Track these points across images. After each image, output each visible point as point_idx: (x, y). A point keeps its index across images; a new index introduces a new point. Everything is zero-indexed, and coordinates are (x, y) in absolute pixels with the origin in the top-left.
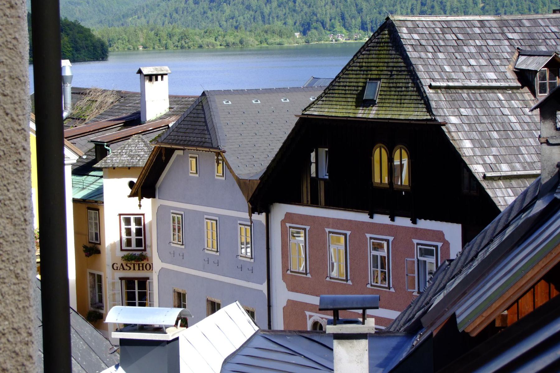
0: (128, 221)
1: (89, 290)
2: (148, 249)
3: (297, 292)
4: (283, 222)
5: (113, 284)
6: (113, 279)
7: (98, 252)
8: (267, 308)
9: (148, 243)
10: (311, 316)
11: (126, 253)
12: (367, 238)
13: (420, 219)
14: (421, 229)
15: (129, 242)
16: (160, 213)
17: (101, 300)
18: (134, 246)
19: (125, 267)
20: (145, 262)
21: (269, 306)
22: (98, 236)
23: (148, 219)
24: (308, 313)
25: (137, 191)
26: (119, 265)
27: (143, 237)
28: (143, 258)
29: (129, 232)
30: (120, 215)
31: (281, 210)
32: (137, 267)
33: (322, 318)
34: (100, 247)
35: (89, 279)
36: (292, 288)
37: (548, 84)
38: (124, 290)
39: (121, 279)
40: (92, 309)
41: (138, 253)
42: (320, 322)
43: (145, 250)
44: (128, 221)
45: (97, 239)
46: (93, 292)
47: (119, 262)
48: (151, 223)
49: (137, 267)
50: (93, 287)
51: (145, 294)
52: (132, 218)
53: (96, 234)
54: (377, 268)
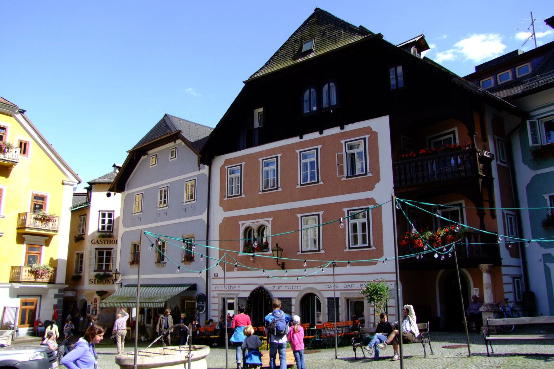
0: (104, 215)
1: (75, 263)
2: (114, 231)
3: (231, 210)
4: (223, 167)
5: (91, 252)
6: (91, 248)
7: (83, 239)
8: (206, 227)
9: (115, 228)
10: (243, 224)
11: (100, 233)
12: (239, 225)
13: (347, 124)
14: (348, 131)
15: (103, 227)
16: (126, 204)
17: (81, 269)
18: (106, 230)
19: (99, 242)
20: (111, 239)
21: (208, 226)
22: (84, 231)
23: (117, 214)
24: (240, 223)
25: (114, 187)
26: (96, 241)
27: (105, 251)
28: (111, 236)
29: (103, 221)
30: (100, 211)
31: (220, 161)
32: (106, 242)
33: (253, 223)
34: (84, 236)
35: (75, 257)
36: (226, 210)
37: (241, 248)
38: (97, 263)
39: (96, 249)
40: (75, 274)
41: (108, 234)
42: (252, 226)
43: (112, 232)
44: (104, 215)
45: (83, 232)
46: (77, 265)
47: (96, 239)
48: (118, 218)
49: (106, 242)
50: (77, 262)
51: (110, 259)
52: (107, 213)
53: (83, 230)
54: (307, 170)
